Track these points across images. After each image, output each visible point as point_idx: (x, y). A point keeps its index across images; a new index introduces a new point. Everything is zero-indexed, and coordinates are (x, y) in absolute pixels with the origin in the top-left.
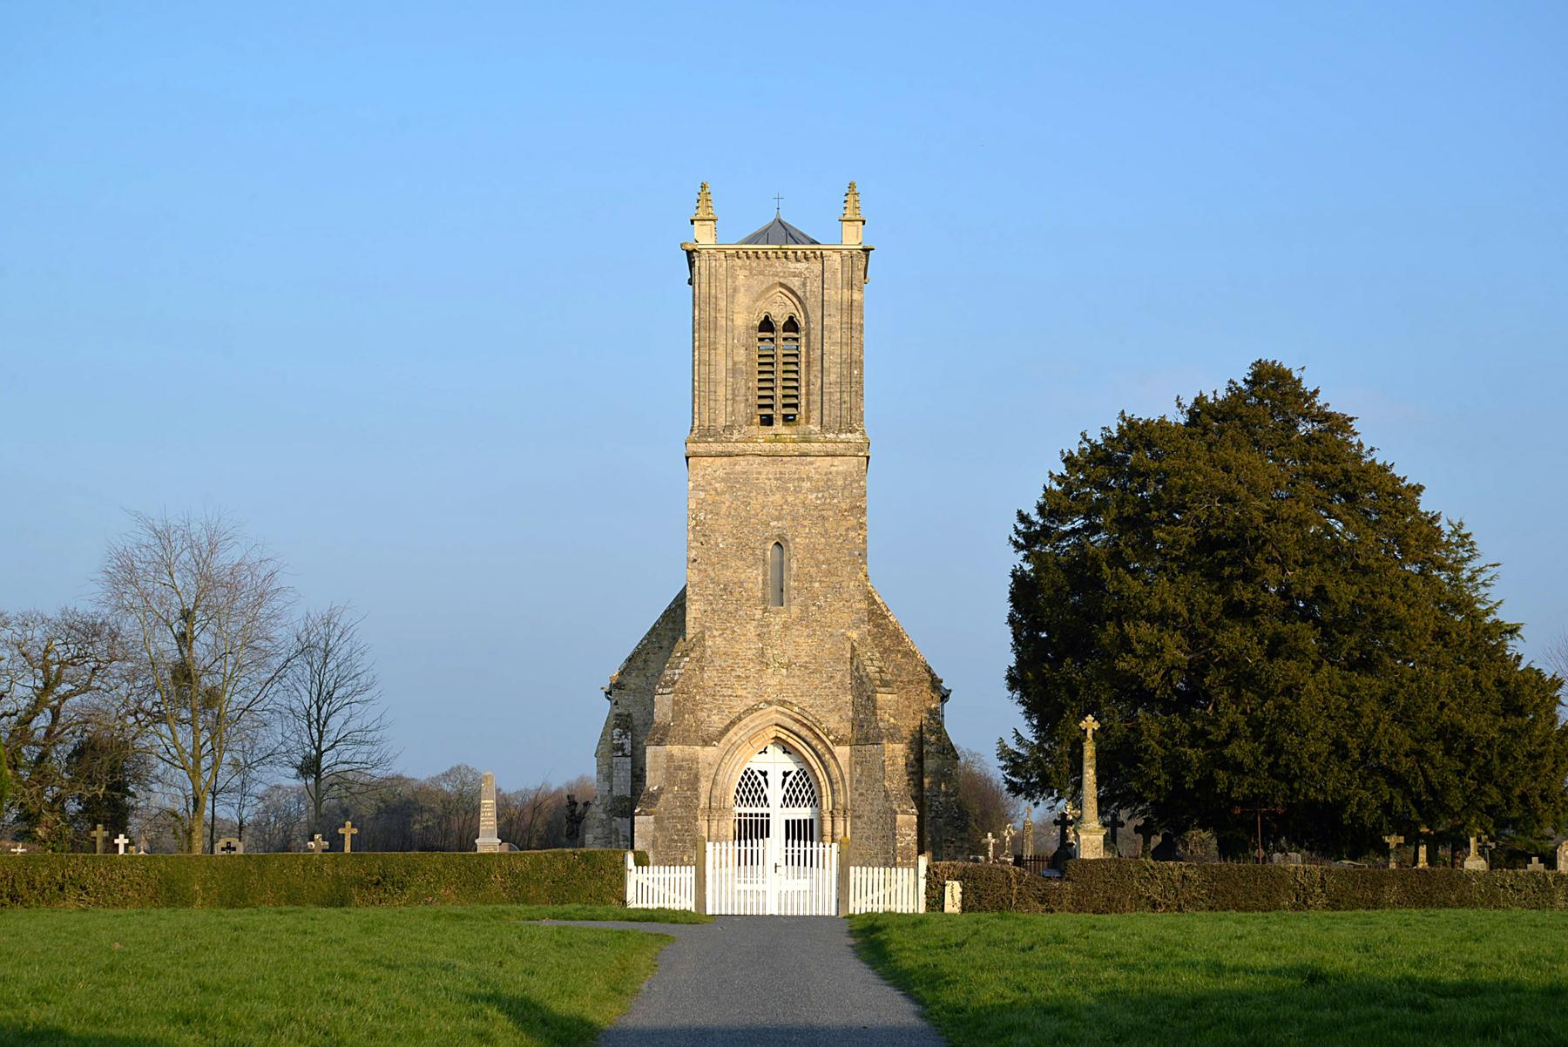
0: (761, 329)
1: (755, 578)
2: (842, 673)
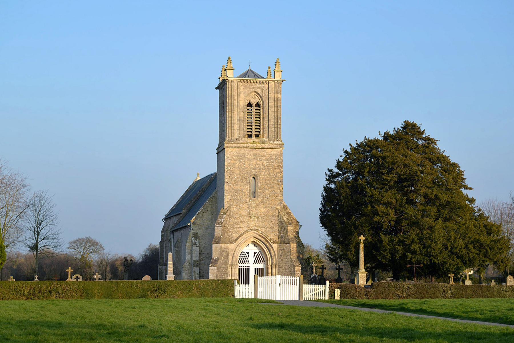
0: (248, 106)
1: (247, 189)
2: (275, 220)
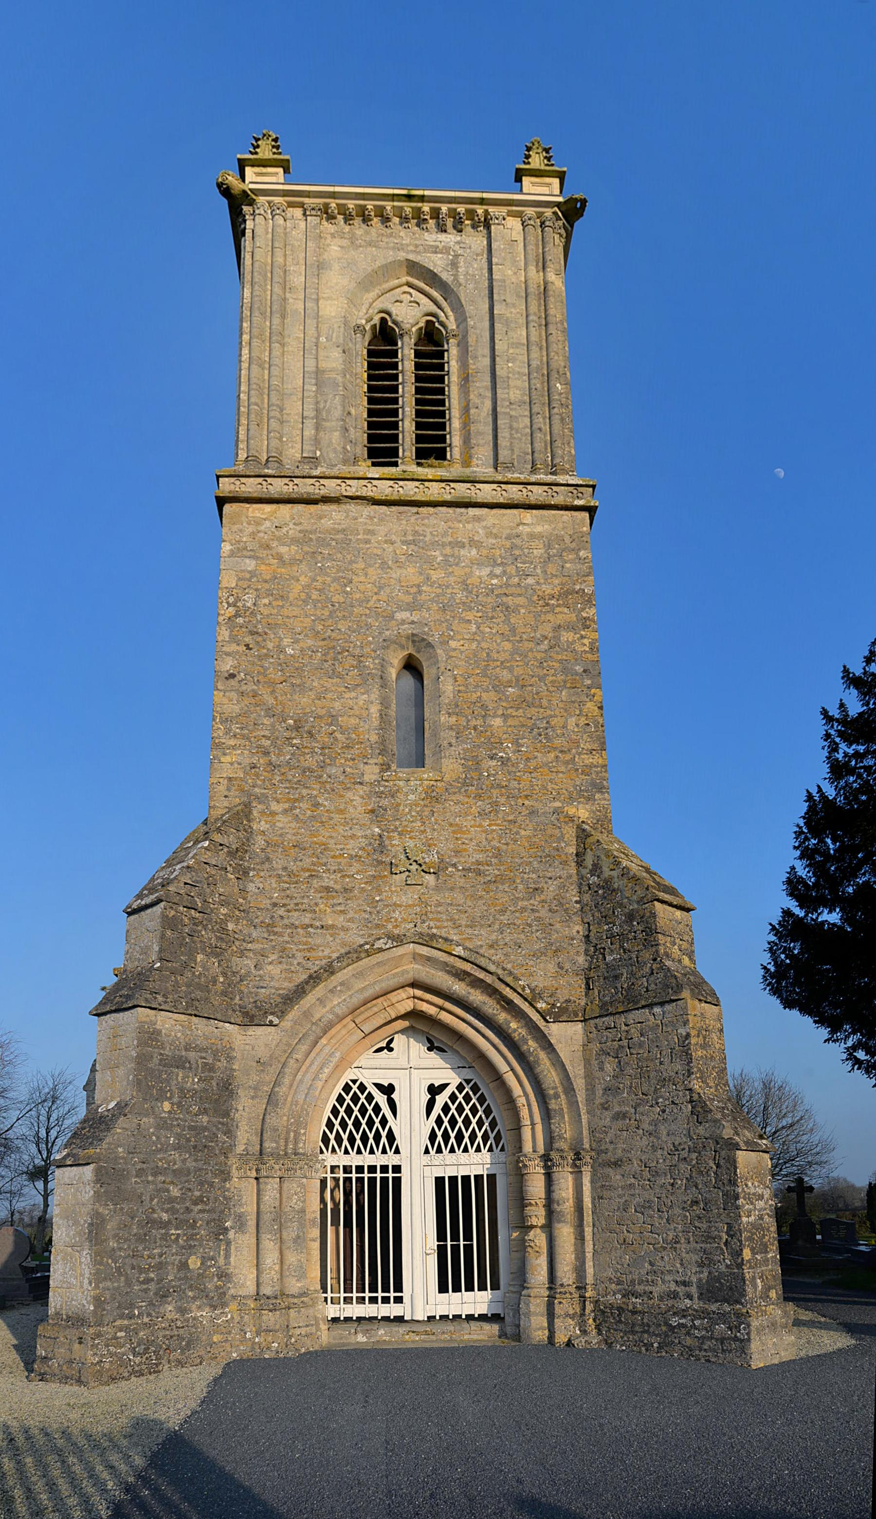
1: (365, 708)
2: (562, 883)
